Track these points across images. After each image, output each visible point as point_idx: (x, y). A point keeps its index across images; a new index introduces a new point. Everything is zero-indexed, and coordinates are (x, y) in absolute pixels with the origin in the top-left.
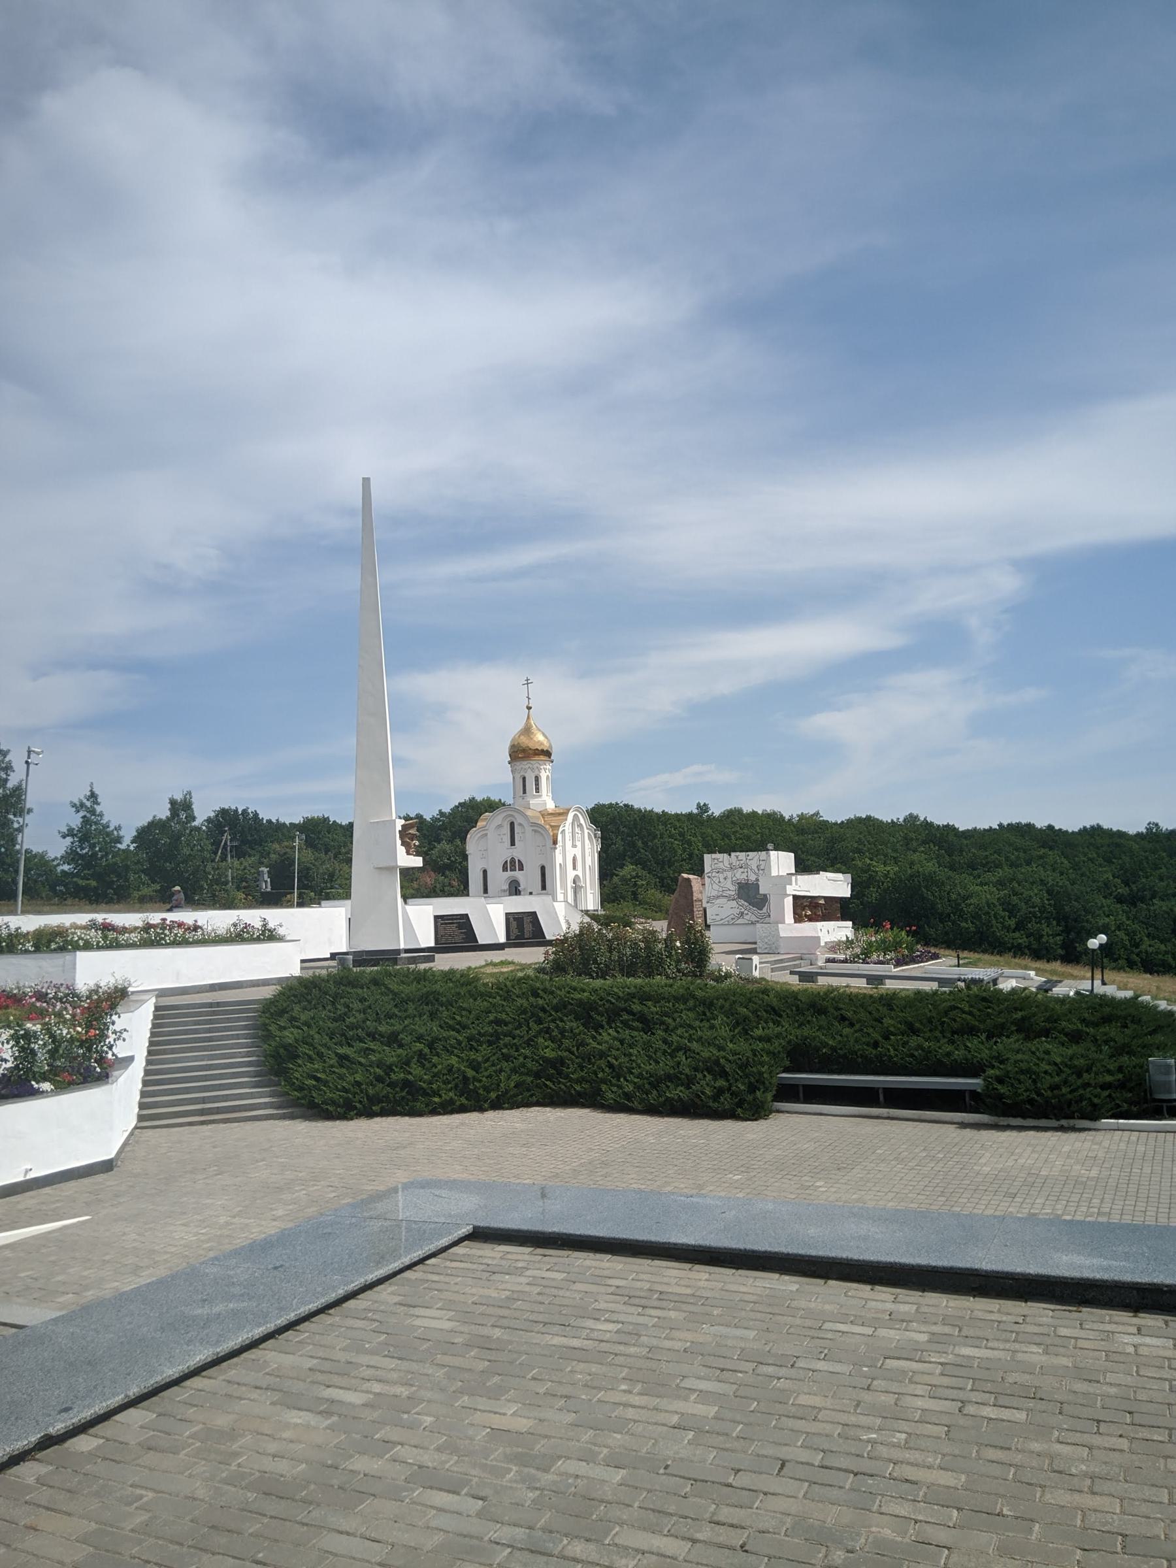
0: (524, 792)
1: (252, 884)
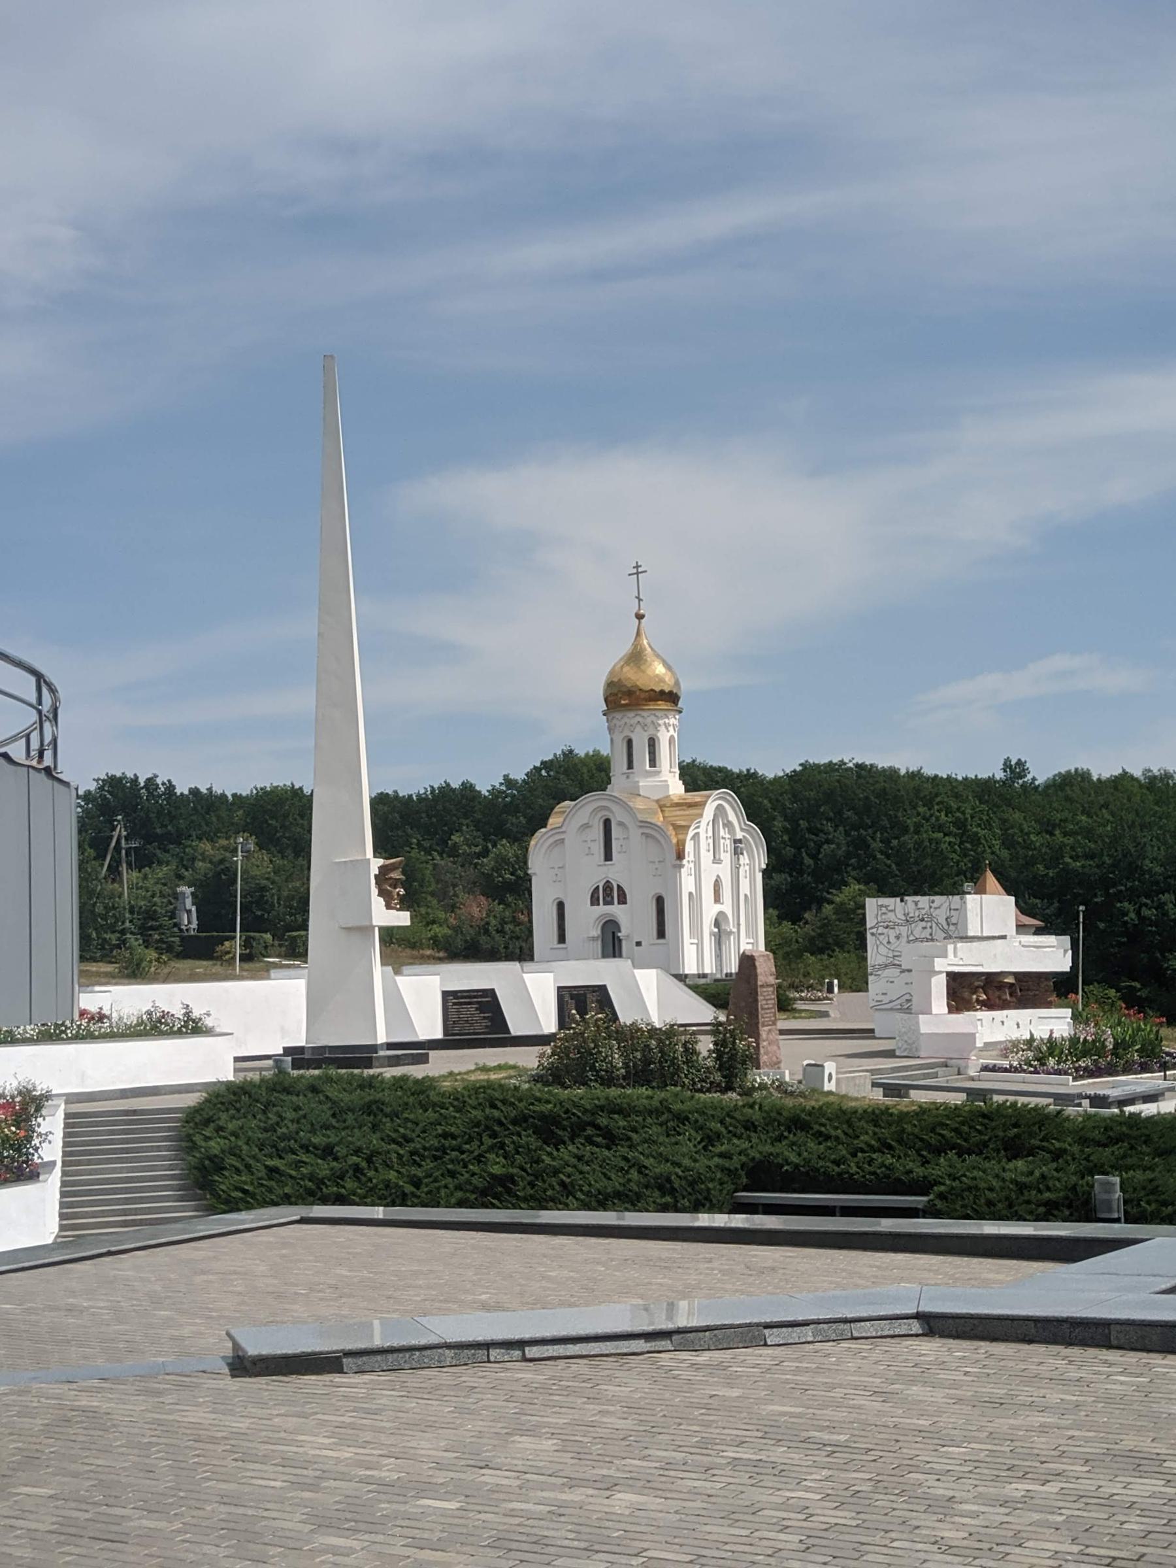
0: (630, 766)
1: (165, 921)
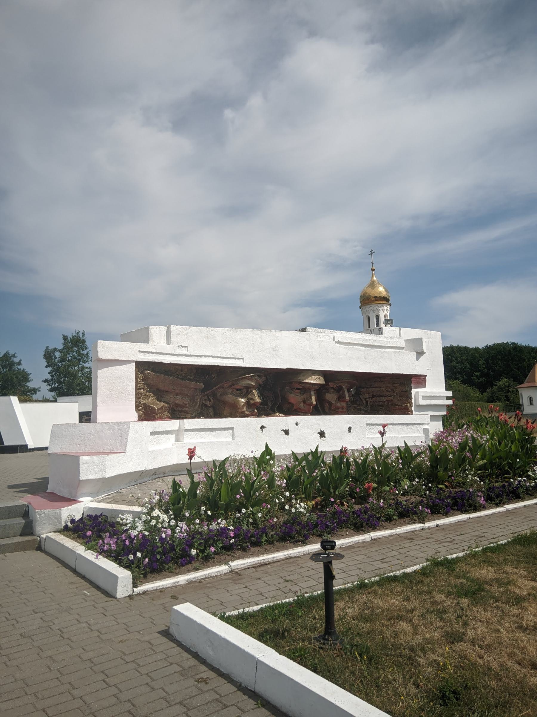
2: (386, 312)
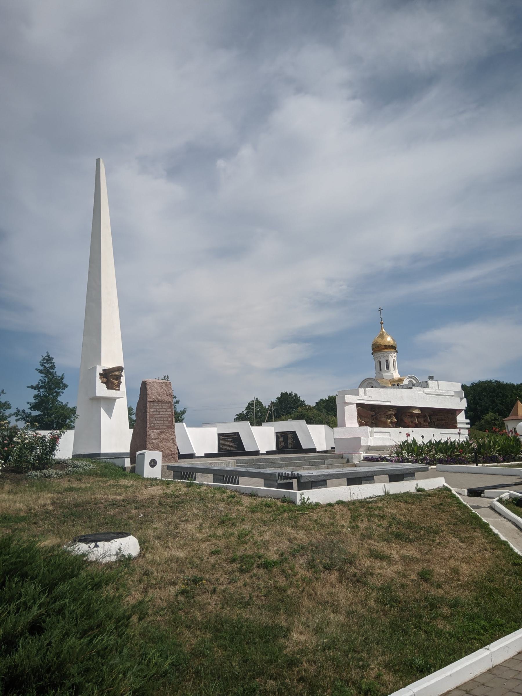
0: (381, 370)
2: (394, 358)
